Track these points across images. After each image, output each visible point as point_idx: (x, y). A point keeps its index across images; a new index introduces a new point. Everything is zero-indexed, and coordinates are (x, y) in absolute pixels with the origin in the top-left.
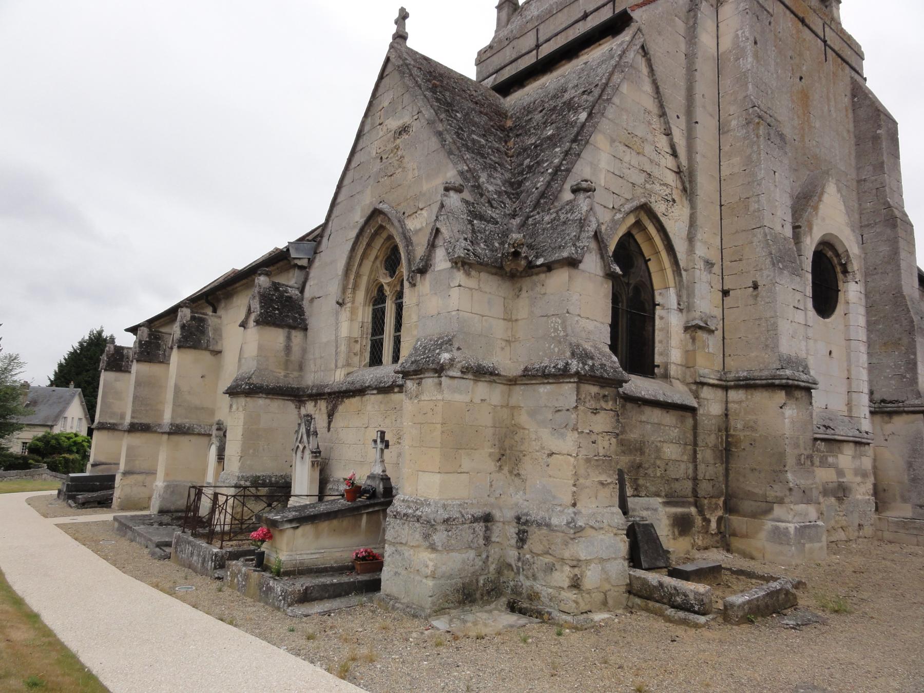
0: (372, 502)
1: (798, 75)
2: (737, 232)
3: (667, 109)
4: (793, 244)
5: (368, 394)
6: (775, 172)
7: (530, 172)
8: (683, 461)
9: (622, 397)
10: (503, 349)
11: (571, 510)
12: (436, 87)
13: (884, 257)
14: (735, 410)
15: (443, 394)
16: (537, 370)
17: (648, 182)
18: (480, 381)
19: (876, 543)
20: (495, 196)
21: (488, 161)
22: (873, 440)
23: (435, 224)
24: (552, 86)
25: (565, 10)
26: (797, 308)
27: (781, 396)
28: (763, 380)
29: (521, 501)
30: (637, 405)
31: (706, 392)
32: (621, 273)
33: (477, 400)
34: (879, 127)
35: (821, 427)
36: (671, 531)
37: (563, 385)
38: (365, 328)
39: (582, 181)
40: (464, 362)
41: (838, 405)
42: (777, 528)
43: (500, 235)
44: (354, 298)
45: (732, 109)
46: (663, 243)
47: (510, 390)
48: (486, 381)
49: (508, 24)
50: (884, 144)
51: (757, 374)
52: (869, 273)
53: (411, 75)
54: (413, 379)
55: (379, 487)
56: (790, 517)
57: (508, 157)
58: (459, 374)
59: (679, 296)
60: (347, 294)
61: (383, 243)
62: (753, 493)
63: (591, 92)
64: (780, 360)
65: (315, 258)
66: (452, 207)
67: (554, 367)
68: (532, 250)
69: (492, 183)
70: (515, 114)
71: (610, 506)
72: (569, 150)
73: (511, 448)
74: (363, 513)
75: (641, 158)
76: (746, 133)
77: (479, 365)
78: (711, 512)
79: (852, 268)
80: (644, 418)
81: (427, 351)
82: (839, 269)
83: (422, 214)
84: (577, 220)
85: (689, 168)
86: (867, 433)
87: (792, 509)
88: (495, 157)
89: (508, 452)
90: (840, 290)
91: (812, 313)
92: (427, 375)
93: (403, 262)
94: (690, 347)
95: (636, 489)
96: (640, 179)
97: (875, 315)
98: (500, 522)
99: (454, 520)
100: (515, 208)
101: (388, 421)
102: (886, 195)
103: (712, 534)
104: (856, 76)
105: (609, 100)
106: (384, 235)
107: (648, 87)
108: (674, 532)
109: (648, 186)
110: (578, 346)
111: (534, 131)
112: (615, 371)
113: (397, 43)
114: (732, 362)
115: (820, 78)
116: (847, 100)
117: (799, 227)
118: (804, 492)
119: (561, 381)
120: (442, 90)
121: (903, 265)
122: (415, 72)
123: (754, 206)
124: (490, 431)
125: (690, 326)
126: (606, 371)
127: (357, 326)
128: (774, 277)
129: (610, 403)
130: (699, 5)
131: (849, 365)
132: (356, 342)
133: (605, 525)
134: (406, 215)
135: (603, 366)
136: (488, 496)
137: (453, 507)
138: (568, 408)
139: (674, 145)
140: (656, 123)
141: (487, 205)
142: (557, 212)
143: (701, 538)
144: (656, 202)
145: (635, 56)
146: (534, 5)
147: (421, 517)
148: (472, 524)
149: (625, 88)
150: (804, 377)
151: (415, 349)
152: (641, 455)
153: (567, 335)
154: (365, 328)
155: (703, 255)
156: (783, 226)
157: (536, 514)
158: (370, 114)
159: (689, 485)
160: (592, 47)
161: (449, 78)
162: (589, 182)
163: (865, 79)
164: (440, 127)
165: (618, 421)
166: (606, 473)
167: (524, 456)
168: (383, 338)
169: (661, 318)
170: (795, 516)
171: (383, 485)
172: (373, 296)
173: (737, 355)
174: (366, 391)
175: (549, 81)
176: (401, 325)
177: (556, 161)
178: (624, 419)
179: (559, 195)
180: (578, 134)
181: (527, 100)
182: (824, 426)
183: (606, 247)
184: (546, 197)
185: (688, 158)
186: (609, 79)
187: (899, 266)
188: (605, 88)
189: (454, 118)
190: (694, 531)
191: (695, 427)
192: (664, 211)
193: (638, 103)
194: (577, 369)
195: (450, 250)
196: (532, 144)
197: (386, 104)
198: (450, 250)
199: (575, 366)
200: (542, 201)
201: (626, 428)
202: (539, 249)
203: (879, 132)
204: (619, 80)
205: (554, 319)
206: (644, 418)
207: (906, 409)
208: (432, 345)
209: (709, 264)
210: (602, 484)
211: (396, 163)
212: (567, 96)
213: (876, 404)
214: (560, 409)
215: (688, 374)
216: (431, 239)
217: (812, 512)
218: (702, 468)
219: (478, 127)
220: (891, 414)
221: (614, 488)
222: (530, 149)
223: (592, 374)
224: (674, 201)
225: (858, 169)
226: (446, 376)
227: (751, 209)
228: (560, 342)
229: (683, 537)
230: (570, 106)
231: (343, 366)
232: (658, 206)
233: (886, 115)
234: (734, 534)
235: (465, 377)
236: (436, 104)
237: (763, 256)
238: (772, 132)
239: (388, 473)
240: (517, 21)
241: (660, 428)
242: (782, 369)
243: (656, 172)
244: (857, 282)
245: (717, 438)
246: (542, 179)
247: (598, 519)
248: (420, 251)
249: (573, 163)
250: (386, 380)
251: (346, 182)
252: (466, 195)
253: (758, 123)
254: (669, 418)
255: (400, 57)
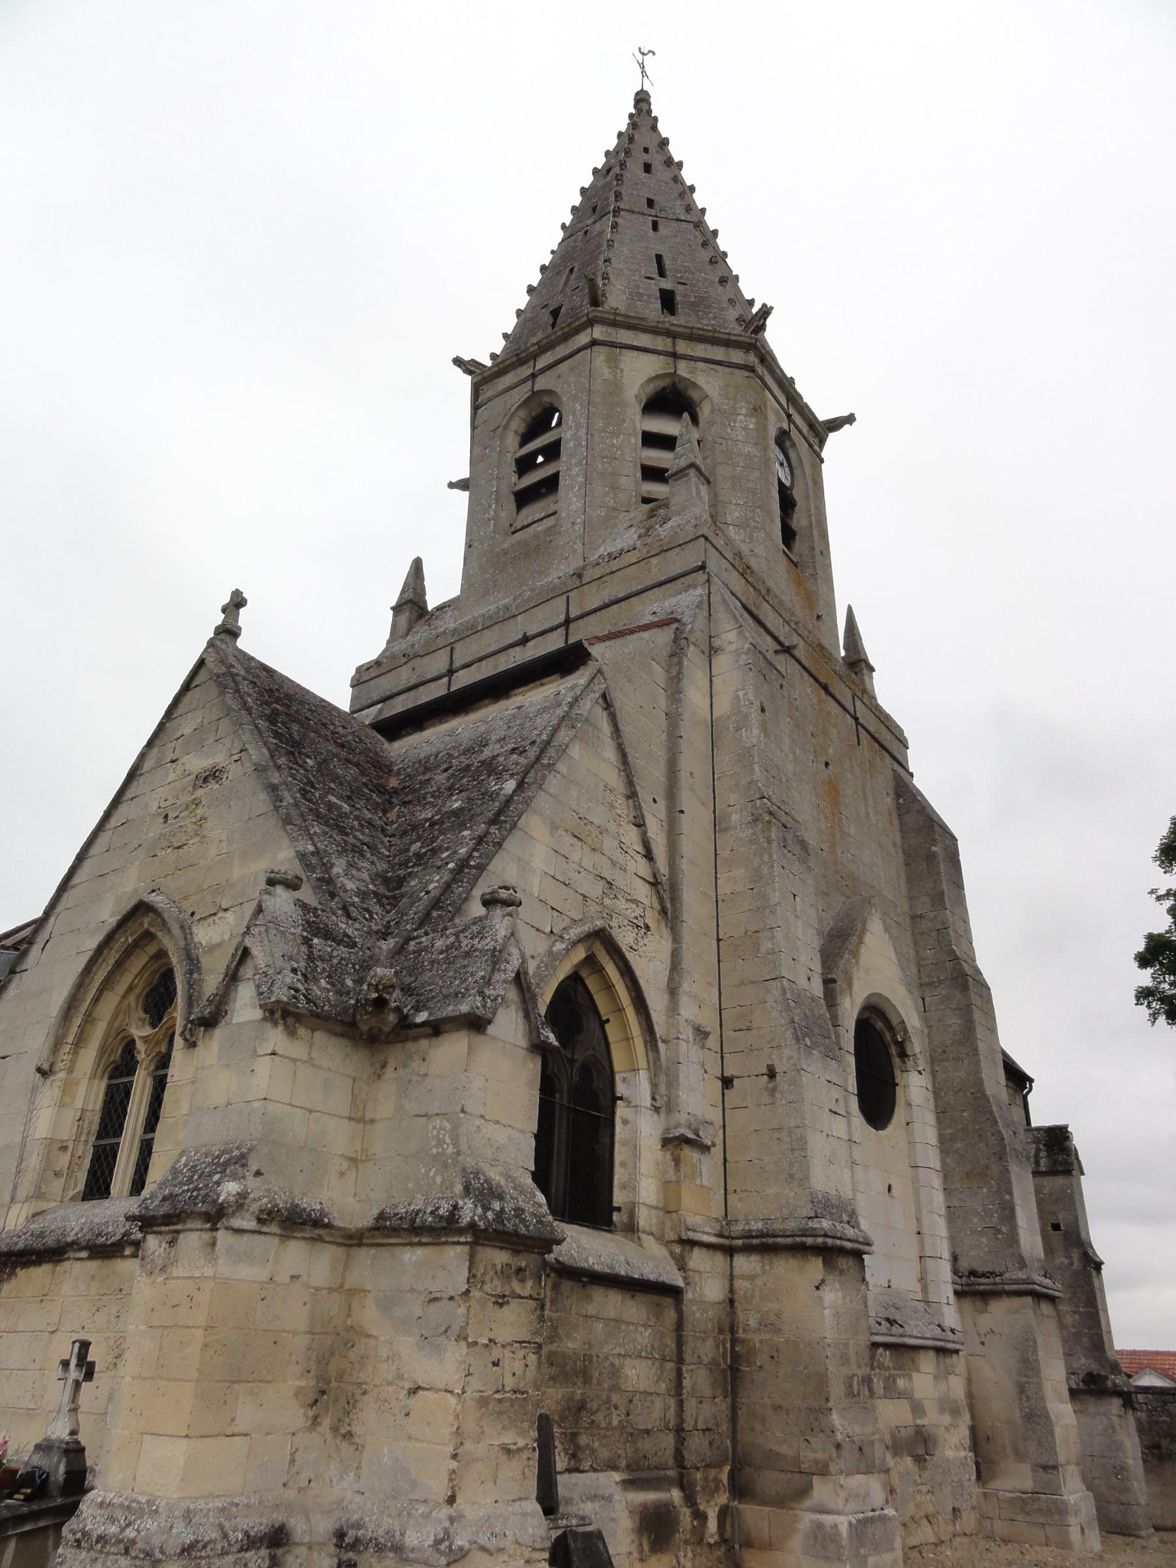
0: (35, 1507)
1: (823, 759)
2: (742, 983)
3: (638, 788)
4: (825, 1007)
5: (68, 1259)
6: (795, 896)
7: (420, 865)
8: (658, 1394)
9: (553, 1269)
10: (342, 1174)
11: (446, 1511)
12: (278, 714)
13: (955, 1035)
14: (745, 1293)
15: (215, 1265)
16: (401, 1218)
17: (607, 895)
18: (294, 1238)
19: (984, 1544)
20: (356, 899)
21: (351, 840)
22: (962, 1344)
23: (243, 941)
24: (466, 735)
25: (496, 628)
26: (835, 1113)
27: (815, 1267)
28: (788, 1236)
29: (349, 1495)
30: (581, 1284)
31: (698, 1259)
32: (557, 1044)
33: (283, 1277)
34: (934, 842)
35: (883, 1322)
36: (636, 1543)
37: (447, 1248)
38: (87, 1122)
39: (500, 888)
40: (265, 1200)
41: (907, 1282)
42: (820, 1526)
43: (357, 967)
44: (73, 1062)
45: (733, 798)
46: (630, 995)
47: (348, 1256)
48: (304, 1238)
49: (407, 635)
50: (942, 867)
51: (778, 1226)
52: (935, 1059)
53: (238, 691)
54: (160, 1233)
55: (57, 1468)
56: (840, 1504)
57: (386, 836)
58: (252, 1224)
59: (654, 1086)
60: (62, 1052)
61: (147, 963)
62: (778, 1454)
63: (525, 751)
64: (812, 1202)
65: (9, 981)
66: (277, 914)
67: (432, 1213)
68: (410, 996)
69: (353, 876)
70: (405, 769)
71: (520, 1499)
72: (485, 836)
73: (341, 1376)
74: (9, 1536)
75: (597, 855)
76: (752, 834)
77: (295, 1206)
78: (708, 1498)
79: (913, 1048)
80: (591, 1309)
81: (196, 1177)
82: (893, 1050)
83: (226, 918)
84: (488, 950)
85: (670, 879)
86: (953, 1331)
87: (842, 1486)
88: (363, 834)
89: (333, 1384)
90: (897, 1084)
91: (858, 1120)
92: (189, 1225)
93: (179, 1000)
94: (671, 1175)
95: (574, 1456)
96: (595, 889)
97: (950, 1127)
98: (301, 1544)
99: (204, 1547)
100: (389, 922)
101: (101, 1318)
102: (951, 941)
103: (709, 1544)
104: (900, 770)
105: (550, 767)
106: (152, 949)
107: (610, 754)
108: (641, 1545)
109: (607, 901)
110: (477, 1174)
111: (432, 800)
112: (540, 1222)
113: (222, 640)
114: (739, 1204)
115: (852, 767)
116: (889, 801)
117: (833, 981)
118: (860, 1449)
119: (443, 1239)
120: (286, 720)
121: (982, 1047)
122: (245, 687)
123: (766, 945)
124: (300, 1343)
125: (671, 1138)
126: (523, 1221)
127: (70, 1116)
128: (799, 1059)
129: (530, 1283)
130: (686, 649)
131: (918, 1211)
132: (64, 1148)
133: (508, 1543)
134: (196, 917)
135: (519, 1211)
136: (284, 1485)
137: (206, 1516)
138: (451, 1294)
139: (648, 842)
140: (622, 807)
141: (340, 912)
142: (457, 935)
143: (690, 1555)
144: (620, 927)
145: (592, 707)
146: (450, 613)
147: (133, 1542)
148: (242, 1555)
149: (575, 751)
150: (850, 1232)
151: (175, 1171)
152: (585, 1383)
153: (458, 1153)
154: (87, 1122)
155: (691, 1018)
156: (809, 979)
157: (377, 1524)
158: (157, 742)
159: (669, 1440)
160: (531, 686)
161: (302, 703)
162: (511, 891)
163: (912, 775)
164: (276, 778)
165: (541, 1318)
166: (516, 1426)
167: (364, 1393)
168: (118, 1144)
169: (625, 1122)
170: (847, 1500)
171: (68, 1464)
172: (112, 1058)
173: (746, 1191)
174: (65, 1253)
175: (463, 727)
176: (157, 1119)
177: (463, 851)
178: (557, 1311)
179: (464, 906)
180: (500, 812)
181: (426, 750)
182: (888, 1320)
183: (534, 998)
184: (442, 907)
185: (669, 863)
186: (552, 735)
187: (976, 1049)
188: (545, 747)
189: (301, 766)
190: (677, 1541)
191: (680, 1326)
192: (632, 943)
193: (596, 775)
194: (472, 1218)
195: (264, 988)
196: (427, 820)
197: (187, 730)
198: (264, 988)
199: (469, 1211)
200: (435, 914)
201: (560, 1330)
202: (421, 995)
203: (934, 849)
204: (567, 739)
205: (438, 1121)
206: (591, 1309)
207: (1006, 1287)
208: (209, 1165)
209: (701, 1033)
210: (507, 1451)
211: (191, 828)
212: (487, 753)
213: (964, 1279)
214: (438, 1295)
215: (669, 1224)
216: (233, 966)
217: (875, 1487)
218: (691, 1405)
219: (341, 784)
220: (986, 1296)
221: (529, 1459)
222: (423, 827)
223: (500, 1228)
224: (647, 928)
225: (911, 899)
226: (226, 1228)
227: (763, 949)
228: (446, 1166)
229: (659, 1555)
230: (491, 768)
231: (28, 1199)
232: (624, 933)
233: (941, 827)
234: (748, 1544)
235: (264, 1229)
236: (274, 741)
237: (782, 1025)
238: (789, 836)
239: (83, 1438)
240: (422, 633)
241: (619, 1328)
242: (817, 1217)
243: (620, 880)
244: (920, 1072)
245: (717, 1346)
246: (438, 877)
247: (497, 1530)
248: (211, 983)
249: (490, 857)
250: (110, 1229)
251: (95, 850)
252: (307, 894)
253: (769, 822)
254: (633, 1309)
255: (222, 662)
